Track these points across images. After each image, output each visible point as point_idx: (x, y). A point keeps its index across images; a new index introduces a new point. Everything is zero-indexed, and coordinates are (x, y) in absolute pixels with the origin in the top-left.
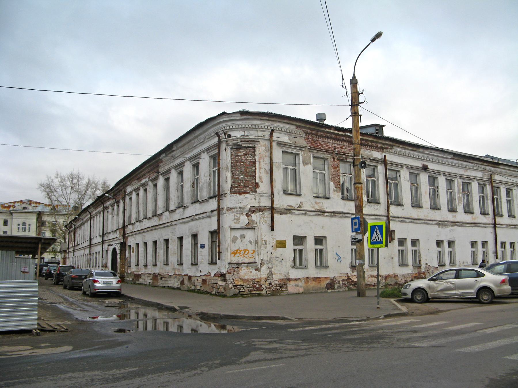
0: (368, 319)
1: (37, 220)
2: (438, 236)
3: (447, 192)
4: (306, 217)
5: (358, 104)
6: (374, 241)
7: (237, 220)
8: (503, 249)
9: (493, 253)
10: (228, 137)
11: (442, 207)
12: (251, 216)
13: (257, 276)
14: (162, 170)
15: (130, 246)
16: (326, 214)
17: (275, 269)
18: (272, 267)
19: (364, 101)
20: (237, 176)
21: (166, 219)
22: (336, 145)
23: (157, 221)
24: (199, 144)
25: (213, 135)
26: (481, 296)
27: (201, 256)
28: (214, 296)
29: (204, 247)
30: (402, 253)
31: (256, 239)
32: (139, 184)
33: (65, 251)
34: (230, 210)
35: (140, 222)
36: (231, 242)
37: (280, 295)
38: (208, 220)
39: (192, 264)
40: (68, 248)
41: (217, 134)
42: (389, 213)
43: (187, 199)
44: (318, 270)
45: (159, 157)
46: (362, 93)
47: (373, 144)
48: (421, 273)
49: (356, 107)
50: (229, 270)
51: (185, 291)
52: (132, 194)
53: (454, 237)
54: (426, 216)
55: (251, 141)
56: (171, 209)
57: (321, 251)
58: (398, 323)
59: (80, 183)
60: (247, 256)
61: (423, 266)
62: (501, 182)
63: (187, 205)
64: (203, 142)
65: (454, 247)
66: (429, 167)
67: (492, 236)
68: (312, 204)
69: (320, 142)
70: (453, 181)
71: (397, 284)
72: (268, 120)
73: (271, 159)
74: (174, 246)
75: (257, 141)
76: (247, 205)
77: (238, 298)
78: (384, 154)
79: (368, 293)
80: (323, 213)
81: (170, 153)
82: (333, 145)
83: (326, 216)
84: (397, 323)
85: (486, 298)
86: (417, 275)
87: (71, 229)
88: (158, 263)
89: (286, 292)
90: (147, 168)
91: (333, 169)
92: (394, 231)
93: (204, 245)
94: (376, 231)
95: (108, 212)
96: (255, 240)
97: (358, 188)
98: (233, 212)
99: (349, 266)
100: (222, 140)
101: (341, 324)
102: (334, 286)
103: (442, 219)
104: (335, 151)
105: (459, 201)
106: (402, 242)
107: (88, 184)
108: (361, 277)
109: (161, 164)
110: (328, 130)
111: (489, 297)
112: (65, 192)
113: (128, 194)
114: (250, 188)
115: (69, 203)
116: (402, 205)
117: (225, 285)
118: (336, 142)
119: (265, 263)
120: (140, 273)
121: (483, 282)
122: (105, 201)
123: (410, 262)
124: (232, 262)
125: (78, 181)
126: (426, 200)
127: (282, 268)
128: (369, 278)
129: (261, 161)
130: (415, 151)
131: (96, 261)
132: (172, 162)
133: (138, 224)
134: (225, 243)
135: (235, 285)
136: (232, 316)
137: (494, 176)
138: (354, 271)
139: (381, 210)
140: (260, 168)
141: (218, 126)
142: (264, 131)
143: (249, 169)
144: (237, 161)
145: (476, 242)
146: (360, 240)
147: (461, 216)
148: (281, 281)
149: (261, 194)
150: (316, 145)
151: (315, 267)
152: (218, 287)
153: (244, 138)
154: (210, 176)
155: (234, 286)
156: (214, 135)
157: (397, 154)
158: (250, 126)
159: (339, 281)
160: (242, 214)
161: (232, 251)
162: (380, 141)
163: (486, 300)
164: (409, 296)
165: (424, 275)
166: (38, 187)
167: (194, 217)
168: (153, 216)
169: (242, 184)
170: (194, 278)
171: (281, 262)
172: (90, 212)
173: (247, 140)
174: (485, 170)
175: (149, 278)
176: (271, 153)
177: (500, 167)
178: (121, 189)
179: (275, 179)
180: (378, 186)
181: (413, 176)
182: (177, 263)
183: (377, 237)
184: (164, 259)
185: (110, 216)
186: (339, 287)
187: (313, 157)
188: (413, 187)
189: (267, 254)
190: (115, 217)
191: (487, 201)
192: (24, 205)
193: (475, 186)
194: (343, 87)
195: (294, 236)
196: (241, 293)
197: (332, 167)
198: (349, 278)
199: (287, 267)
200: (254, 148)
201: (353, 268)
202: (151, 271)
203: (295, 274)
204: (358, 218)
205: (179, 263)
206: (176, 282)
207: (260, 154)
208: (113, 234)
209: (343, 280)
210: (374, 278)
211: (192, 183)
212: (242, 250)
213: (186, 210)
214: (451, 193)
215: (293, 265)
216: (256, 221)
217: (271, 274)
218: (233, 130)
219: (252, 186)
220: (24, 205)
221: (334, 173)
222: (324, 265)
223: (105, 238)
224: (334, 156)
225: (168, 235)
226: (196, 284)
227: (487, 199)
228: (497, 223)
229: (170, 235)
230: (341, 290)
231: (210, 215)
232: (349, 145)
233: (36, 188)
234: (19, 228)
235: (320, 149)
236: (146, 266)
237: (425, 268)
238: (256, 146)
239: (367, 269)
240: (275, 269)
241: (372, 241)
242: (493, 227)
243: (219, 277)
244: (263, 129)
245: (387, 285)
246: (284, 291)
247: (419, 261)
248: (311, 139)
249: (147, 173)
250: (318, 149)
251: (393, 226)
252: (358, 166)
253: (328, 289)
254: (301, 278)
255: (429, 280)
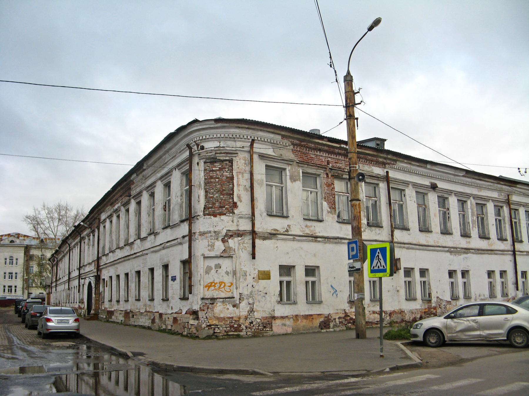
0: (368, 373)
1: (25, 254)
2: (450, 265)
3: (459, 215)
4: (295, 242)
5: (354, 105)
6: (375, 268)
7: (211, 247)
8: (524, 280)
9: (513, 284)
10: (200, 149)
11: (454, 231)
12: (228, 242)
13: (235, 313)
14: (133, 193)
15: (104, 279)
16: (319, 239)
17: (257, 306)
18: (254, 303)
19: (361, 102)
20: (211, 194)
21: (138, 248)
22: (329, 159)
23: (129, 251)
24: (170, 160)
25: (184, 147)
26: (512, 338)
27: (172, 290)
28: (186, 339)
29: (175, 279)
30: (409, 285)
31: (234, 270)
32: (112, 210)
33: (49, 286)
34: (203, 235)
35: (113, 253)
36: (205, 273)
37: (263, 336)
38: (180, 247)
39: (163, 300)
40: (52, 283)
41: (188, 146)
42: (393, 238)
43: (158, 224)
44: (309, 305)
45: (130, 178)
46: (358, 92)
47: (374, 158)
48: (432, 308)
49: (351, 109)
50: (201, 306)
51: (156, 331)
52: (106, 222)
53: (468, 266)
54: (435, 242)
55: (227, 153)
56: (142, 236)
57: (313, 283)
58: (409, 381)
59: (67, 215)
60: (223, 289)
61: (434, 300)
62: (520, 204)
63: (158, 231)
64: (174, 157)
65: (469, 277)
66: (439, 186)
67: (512, 264)
68: (302, 228)
69: (311, 155)
70: (465, 201)
71: (403, 321)
72: (248, 128)
73: (252, 174)
74: (145, 279)
75: (234, 153)
76: (223, 228)
77: (212, 340)
78: (386, 170)
79: (369, 334)
80: (315, 238)
81: (141, 172)
82: (326, 158)
83: (319, 241)
84: (409, 381)
85: (520, 341)
86: (427, 310)
87: (55, 262)
88: (130, 299)
89: (271, 333)
90: (119, 191)
91: (326, 187)
92: (399, 259)
93: (175, 276)
94: (378, 256)
95: (84, 242)
96: (233, 270)
97: (356, 205)
98: (207, 237)
99: (346, 301)
100: (194, 153)
101: (330, 382)
102: (329, 325)
103: (455, 246)
104: (329, 166)
105: (473, 225)
106: (408, 272)
107: (77, 215)
108: (360, 315)
109: (133, 186)
110: (321, 142)
111: (524, 339)
112: (52, 224)
113: (102, 222)
114: (227, 209)
115: (56, 236)
116: (408, 230)
117: (198, 324)
118: (330, 155)
119: (245, 298)
120: (113, 310)
121: (515, 320)
122: (82, 231)
123: (419, 295)
124: (206, 297)
125: (66, 213)
126: (435, 223)
127: (266, 303)
128: (370, 314)
129: (240, 176)
130: (422, 166)
131: (74, 296)
132: (144, 183)
133: (111, 254)
134: (197, 274)
135: (208, 324)
136: (188, 368)
137: (512, 197)
138: (352, 307)
139: (383, 234)
140: (238, 185)
141: (188, 138)
142: (244, 142)
143: (225, 186)
144: (211, 177)
145: (493, 271)
146: (359, 269)
147: (476, 242)
148: (265, 319)
149: (239, 216)
150: (305, 158)
151: (306, 303)
152: (190, 327)
153: (219, 150)
154: (181, 196)
155: (208, 326)
156: (186, 148)
157: (401, 170)
158: (226, 135)
159: (335, 319)
160: (217, 239)
161: (206, 284)
162: (382, 155)
163: (520, 343)
164: (420, 339)
165: (435, 311)
166: (23, 220)
167: (165, 245)
168: (125, 245)
169: (217, 204)
170: (164, 315)
171: (264, 297)
172: (69, 243)
173: (223, 152)
174: (500, 191)
175: (121, 316)
176: (252, 167)
177: (518, 186)
178: (95, 216)
179: (256, 198)
180: (380, 207)
181: (419, 196)
182: (148, 299)
183: (379, 263)
184: (135, 294)
185: (86, 247)
186: (335, 326)
187: (303, 173)
188: (421, 209)
189: (247, 287)
190: (91, 247)
191: (504, 225)
192: (11, 239)
193: (490, 208)
194: (331, 66)
195: (279, 265)
196: (216, 334)
197: (326, 184)
198: (346, 315)
199: (271, 303)
200: (231, 162)
201: (351, 302)
202: (123, 308)
203: (281, 311)
204: (356, 242)
205: (151, 298)
206: (147, 320)
207: (238, 168)
208: (89, 267)
209: (339, 318)
210: (376, 315)
211: (164, 206)
212: (217, 283)
213: (157, 237)
214: (464, 215)
215: (279, 300)
216: (234, 248)
217: (252, 311)
218: (207, 140)
219: (229, 206)
220: (11, 239)
221: (328, 192)
222: (317, 300)
223: (82, 271)
224: (328, 172)
225: (140, 266)
226: (167, 322)
227: (505, 223)
228: (516, 250)
229: (142, 266)
230: (337, 329)
231: (181, 242)
232: (345, 160)
233: (22, 221)
234: (6, 262)
235: (311, 163)
236: (118, 301)
237: (436, 302)
238: (234, 158)
239: (369, 304)
240: (257, 306)
241: (372, 269)
242: (512, 255)
243: (190, 314)
244: (241, 138)
245: (391, 324)
246: (268, 332)
247: (429, 294)
248: (299, 151)
249: (119, 197)
250: (308, 163)
251: (398, 253)
252: (354, 179)
253: (322, 329)
254: (290, 316)
255: (445, 318)
